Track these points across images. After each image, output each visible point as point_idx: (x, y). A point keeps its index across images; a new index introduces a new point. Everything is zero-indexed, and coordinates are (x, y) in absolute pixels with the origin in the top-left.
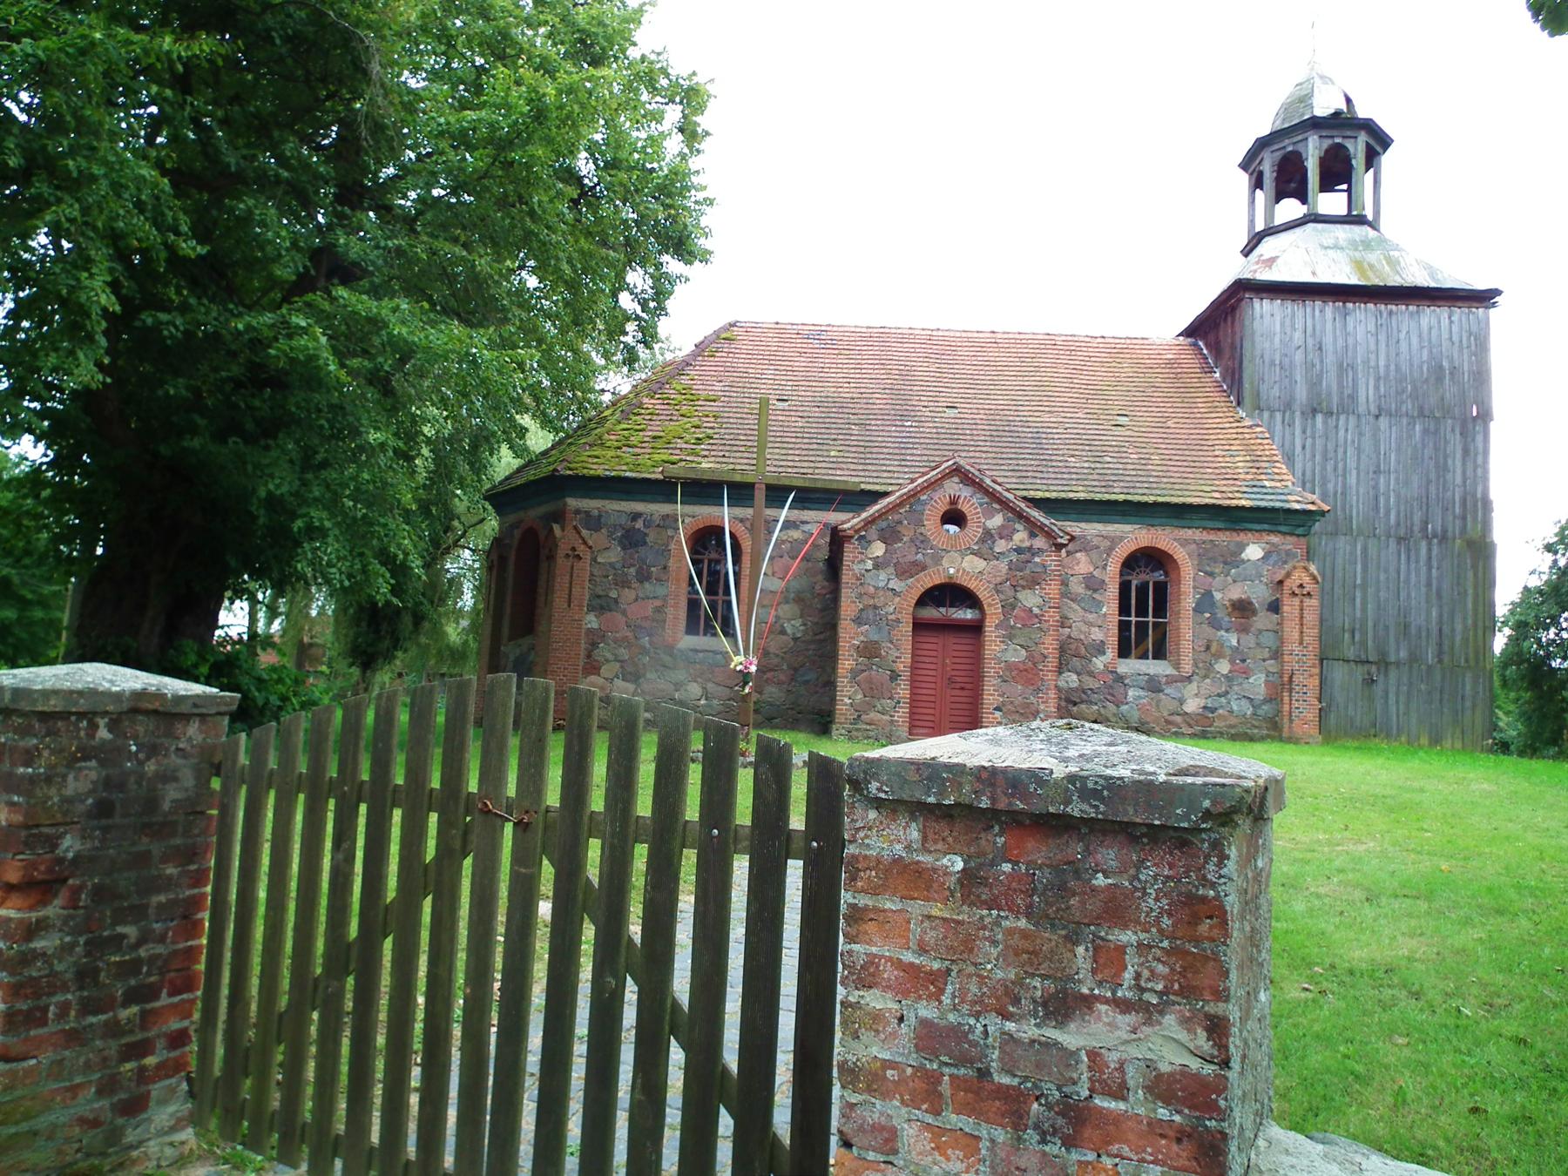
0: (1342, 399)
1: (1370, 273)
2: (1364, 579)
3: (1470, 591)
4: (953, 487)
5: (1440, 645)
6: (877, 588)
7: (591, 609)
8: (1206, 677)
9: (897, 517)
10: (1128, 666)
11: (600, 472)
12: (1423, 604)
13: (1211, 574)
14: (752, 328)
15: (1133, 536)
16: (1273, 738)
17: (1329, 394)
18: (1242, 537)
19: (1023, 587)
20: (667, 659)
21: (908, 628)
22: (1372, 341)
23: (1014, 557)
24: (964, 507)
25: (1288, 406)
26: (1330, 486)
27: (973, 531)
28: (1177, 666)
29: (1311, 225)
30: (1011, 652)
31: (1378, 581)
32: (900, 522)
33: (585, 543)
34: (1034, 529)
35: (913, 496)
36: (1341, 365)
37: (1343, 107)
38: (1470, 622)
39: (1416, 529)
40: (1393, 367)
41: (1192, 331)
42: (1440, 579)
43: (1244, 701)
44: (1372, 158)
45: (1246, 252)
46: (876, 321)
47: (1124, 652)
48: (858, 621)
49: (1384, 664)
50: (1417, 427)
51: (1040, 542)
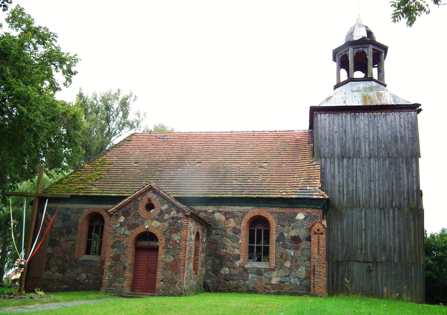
0: (354, 152)
3: (412, 230)
5: (400, 254)
6: (120, 234)
7: (50, 245)
8: (281, 269)
9: (129, 207)
13: (283, 226)
15: (252, 211)
16: (307, 294)
17: (349, 150)
18: (296, 210)
19: (174, 233)
20: (75, 264)
23: (171, 221)
24: (154, 202)
26: (350, 188)
29: (350, 83)
31: (372, 228)
32: (130, 209)
34: (179, 210)
35: (135, 198)
36: (354, 138)
40: (376, 138)
42: (398, 225)
43: (296, 279)
48: (113, 247)
49: (375, 262)
50: (387, 162)
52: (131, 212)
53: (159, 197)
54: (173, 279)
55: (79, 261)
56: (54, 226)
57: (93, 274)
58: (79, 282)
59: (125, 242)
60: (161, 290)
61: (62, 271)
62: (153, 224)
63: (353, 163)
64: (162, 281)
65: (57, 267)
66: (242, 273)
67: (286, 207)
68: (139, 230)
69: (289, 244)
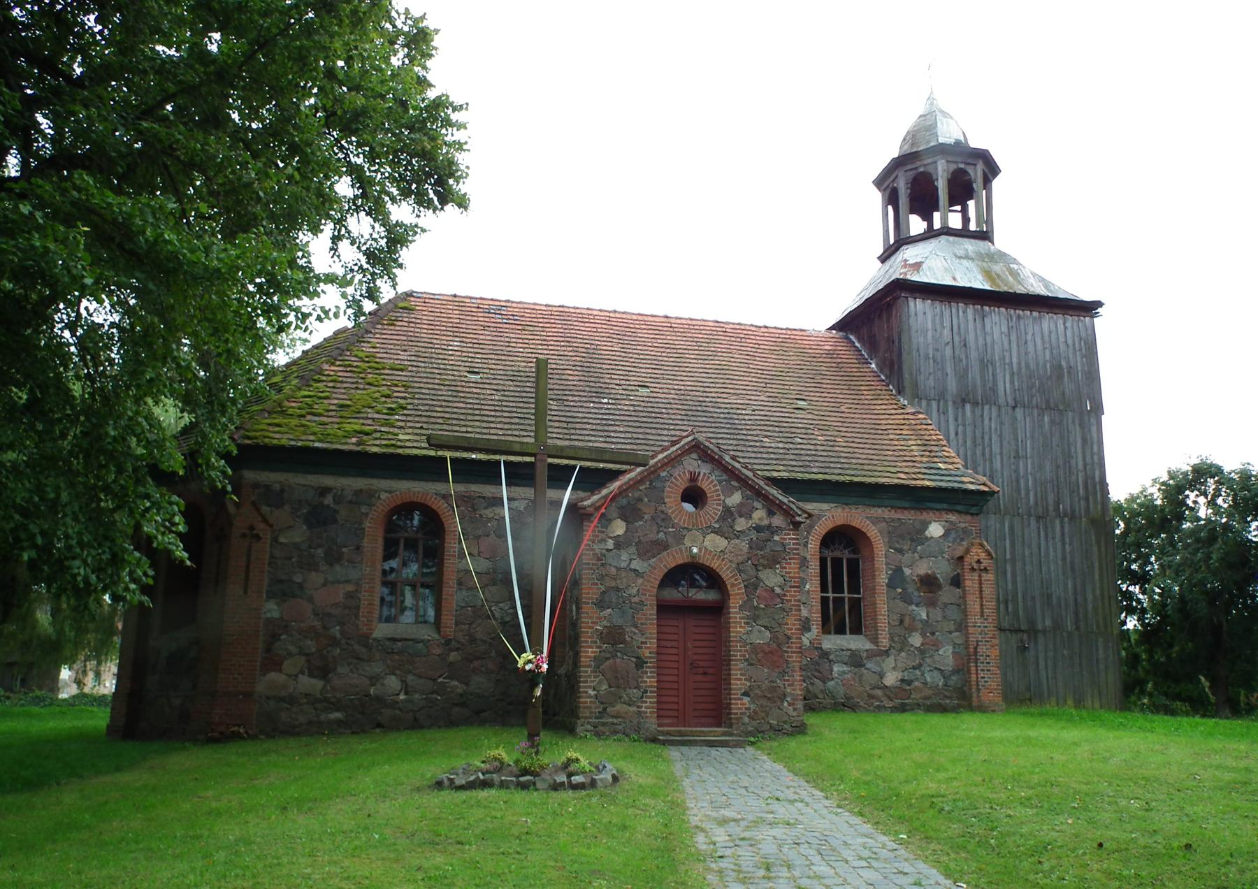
1: (998, 281)
2: (1013, 553)
3: (1096, 564)
4: (692, 464)
5: (1076, 613)
6: (618, 569)
7: (271, 595)
8: (901, 650)
9: (637, 494)
10: (831, 642)
11: (284, 442)
12: (1061, 577)
13: (900, 551)
14: (428, 299)
15: (829, 514)
17: (974, 387)
18: (925, 516)
19: (765, 567)
21: (651, 611)
22: (1006, 341)
23: (754, 535)
24: (704, 484)
25: (941, 396)
27: (713, 509)
28: (875, 640)
29: (944, 238)
30: (756, 633)
32: (640, 500)
33: (265, 521)
34: (773, 507)
36: (982, 361)
37: (962, 138)
38: (1098, 592)
39: (1051, 508)
41: (847, 325)
43: (936, 673)
44: (987, 182)
45: (884, 259)
46: (555, 301)
47: (825, 629)
48: (601, 604)
49: (1033, 632)
51: (778, 521)
52: (645, 509)
53: (717, 473)
54: (774, 689)
55: (375, 639)
56: (282, 540)
57: (420, 677)
58: (379, 699)
59: (634, 591)
60: (746, 720)
61: (323, 671)
62: (706, 543)
63: (982, 416)
64: (746, 694)
65: (303, 659)
66: (817, 664)
67: (905, 508)
68: (671, 559)
69: (916, 593)
